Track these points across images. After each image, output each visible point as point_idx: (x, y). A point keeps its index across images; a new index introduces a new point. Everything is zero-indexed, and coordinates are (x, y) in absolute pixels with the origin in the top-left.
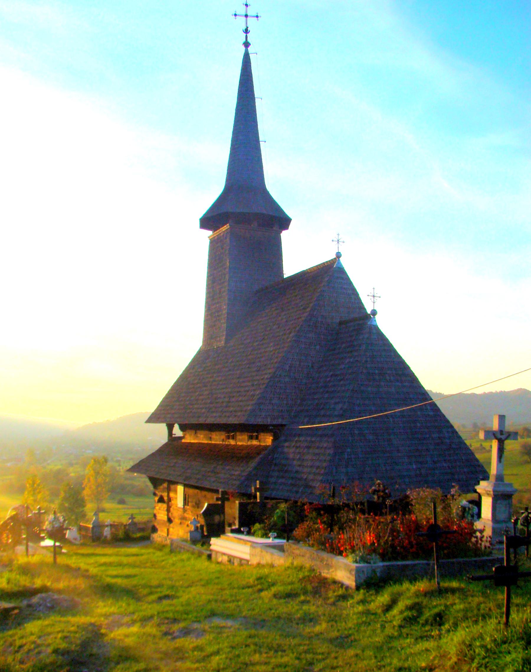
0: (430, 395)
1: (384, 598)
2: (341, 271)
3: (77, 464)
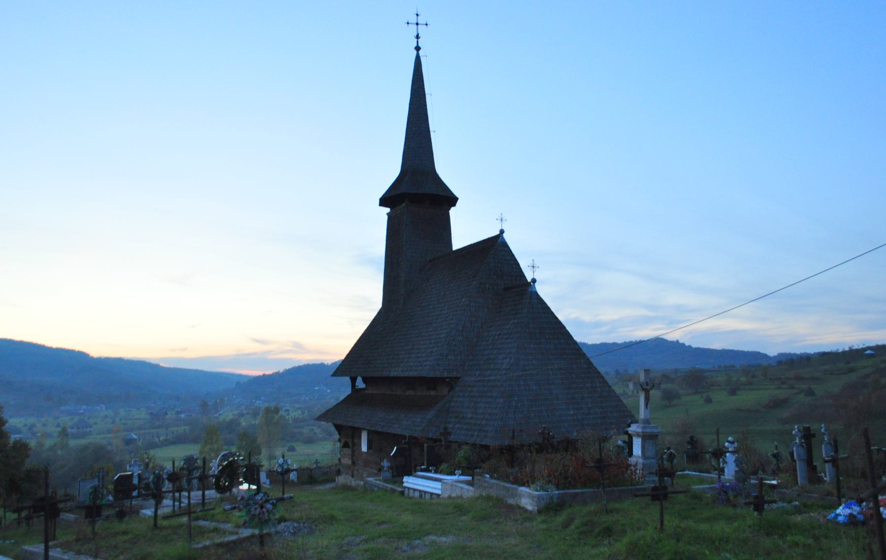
0: (584, 350)
1: (560, 519)
2: (505, 245)
3: (248, 414)
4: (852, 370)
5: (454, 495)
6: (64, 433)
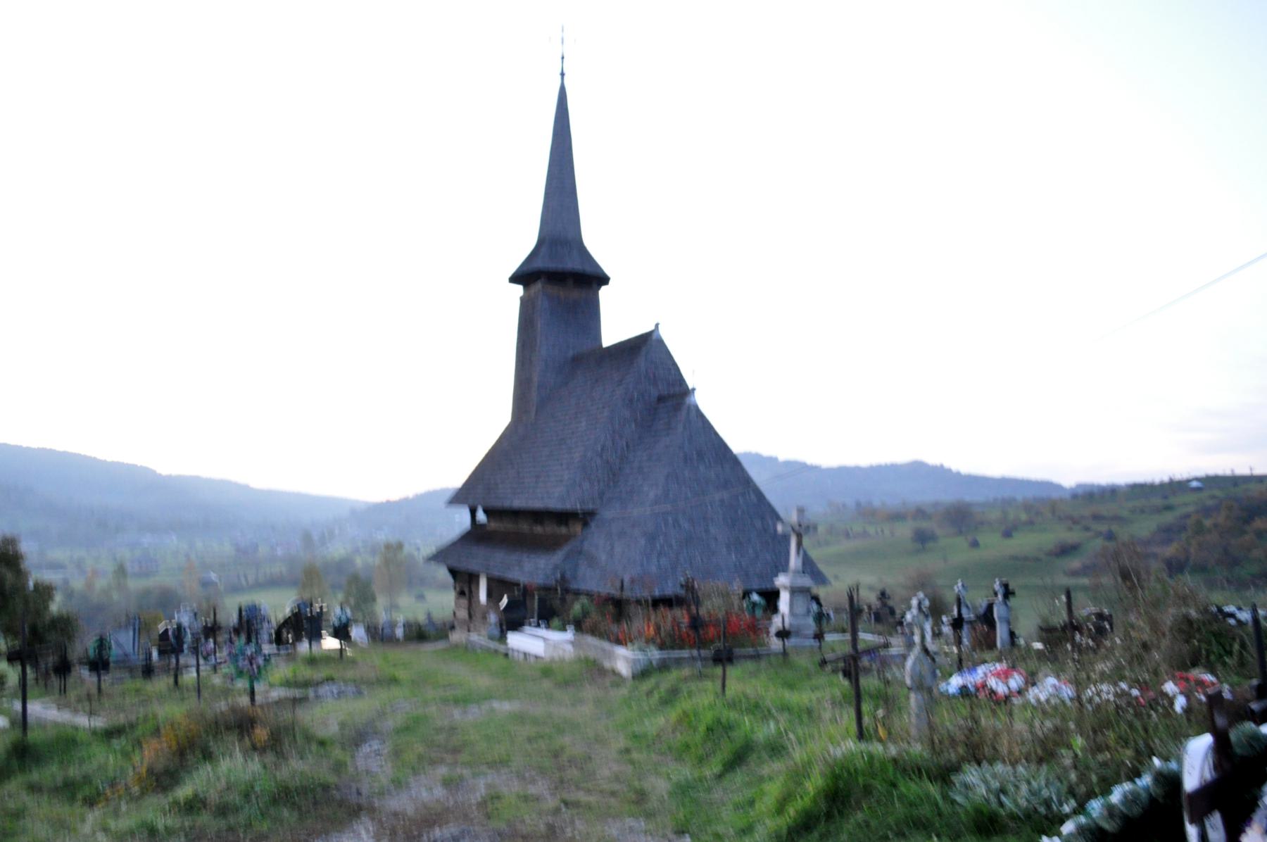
0: (758, 477)
2: (661, 342)
4: (1169, 508)
6: (121, 571)
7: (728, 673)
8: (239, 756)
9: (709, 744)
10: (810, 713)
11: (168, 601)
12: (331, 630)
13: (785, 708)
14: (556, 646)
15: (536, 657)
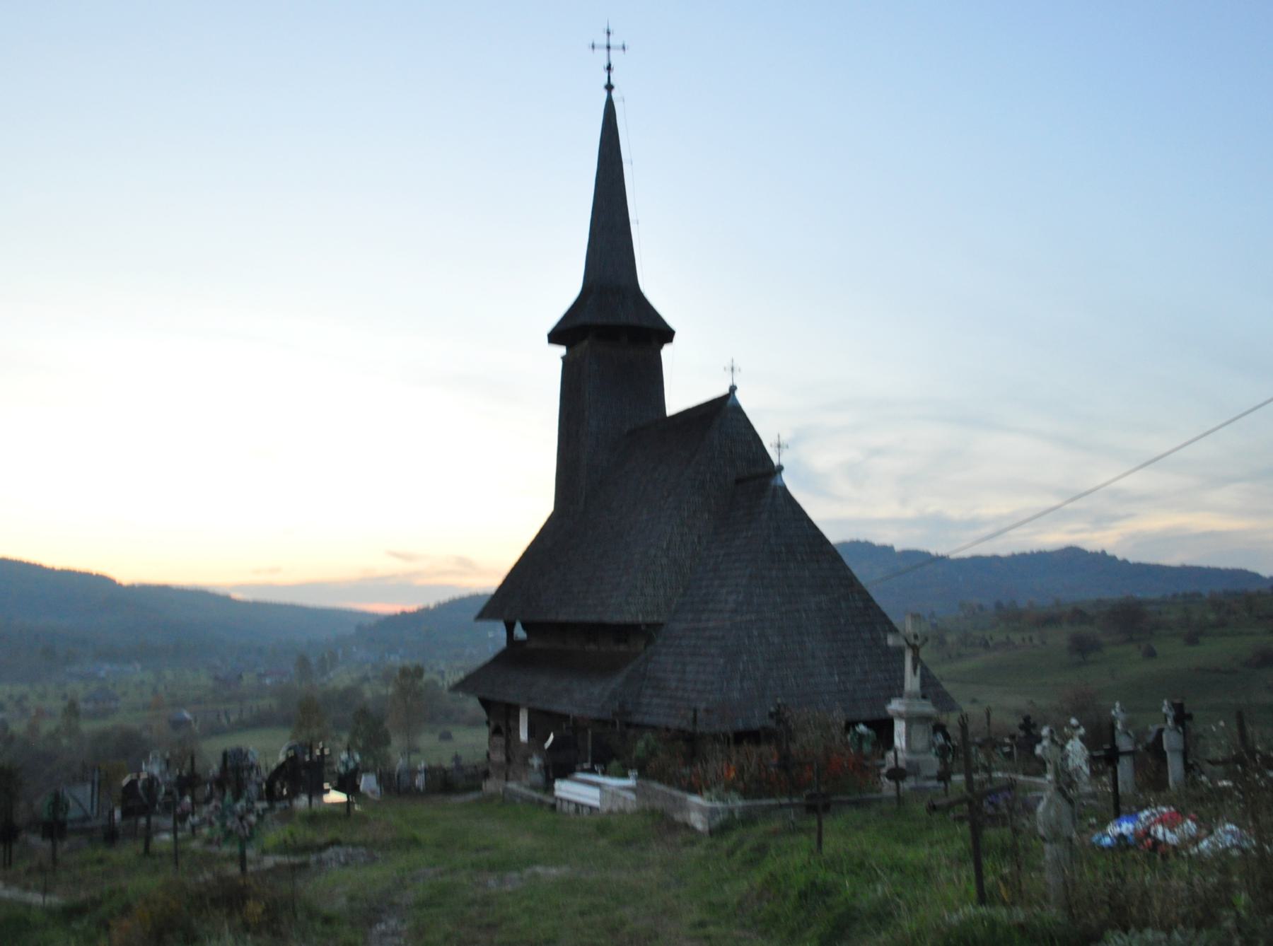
1: (726, 844)
5: (615, 808)
6: (72, 710)
7: (825, 824)
8: (229, 939)
9: (803, 914)
10: (927, 872)
11: (130, 747)
12: (335, 782)
13: (897, 867)
14: (614, 795)
15: (591, 808)
